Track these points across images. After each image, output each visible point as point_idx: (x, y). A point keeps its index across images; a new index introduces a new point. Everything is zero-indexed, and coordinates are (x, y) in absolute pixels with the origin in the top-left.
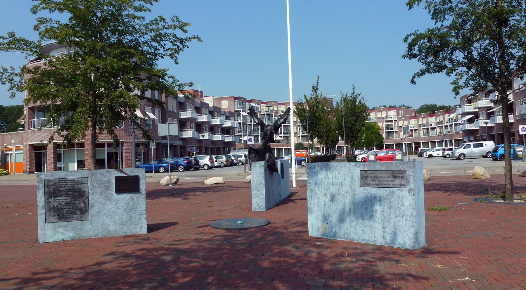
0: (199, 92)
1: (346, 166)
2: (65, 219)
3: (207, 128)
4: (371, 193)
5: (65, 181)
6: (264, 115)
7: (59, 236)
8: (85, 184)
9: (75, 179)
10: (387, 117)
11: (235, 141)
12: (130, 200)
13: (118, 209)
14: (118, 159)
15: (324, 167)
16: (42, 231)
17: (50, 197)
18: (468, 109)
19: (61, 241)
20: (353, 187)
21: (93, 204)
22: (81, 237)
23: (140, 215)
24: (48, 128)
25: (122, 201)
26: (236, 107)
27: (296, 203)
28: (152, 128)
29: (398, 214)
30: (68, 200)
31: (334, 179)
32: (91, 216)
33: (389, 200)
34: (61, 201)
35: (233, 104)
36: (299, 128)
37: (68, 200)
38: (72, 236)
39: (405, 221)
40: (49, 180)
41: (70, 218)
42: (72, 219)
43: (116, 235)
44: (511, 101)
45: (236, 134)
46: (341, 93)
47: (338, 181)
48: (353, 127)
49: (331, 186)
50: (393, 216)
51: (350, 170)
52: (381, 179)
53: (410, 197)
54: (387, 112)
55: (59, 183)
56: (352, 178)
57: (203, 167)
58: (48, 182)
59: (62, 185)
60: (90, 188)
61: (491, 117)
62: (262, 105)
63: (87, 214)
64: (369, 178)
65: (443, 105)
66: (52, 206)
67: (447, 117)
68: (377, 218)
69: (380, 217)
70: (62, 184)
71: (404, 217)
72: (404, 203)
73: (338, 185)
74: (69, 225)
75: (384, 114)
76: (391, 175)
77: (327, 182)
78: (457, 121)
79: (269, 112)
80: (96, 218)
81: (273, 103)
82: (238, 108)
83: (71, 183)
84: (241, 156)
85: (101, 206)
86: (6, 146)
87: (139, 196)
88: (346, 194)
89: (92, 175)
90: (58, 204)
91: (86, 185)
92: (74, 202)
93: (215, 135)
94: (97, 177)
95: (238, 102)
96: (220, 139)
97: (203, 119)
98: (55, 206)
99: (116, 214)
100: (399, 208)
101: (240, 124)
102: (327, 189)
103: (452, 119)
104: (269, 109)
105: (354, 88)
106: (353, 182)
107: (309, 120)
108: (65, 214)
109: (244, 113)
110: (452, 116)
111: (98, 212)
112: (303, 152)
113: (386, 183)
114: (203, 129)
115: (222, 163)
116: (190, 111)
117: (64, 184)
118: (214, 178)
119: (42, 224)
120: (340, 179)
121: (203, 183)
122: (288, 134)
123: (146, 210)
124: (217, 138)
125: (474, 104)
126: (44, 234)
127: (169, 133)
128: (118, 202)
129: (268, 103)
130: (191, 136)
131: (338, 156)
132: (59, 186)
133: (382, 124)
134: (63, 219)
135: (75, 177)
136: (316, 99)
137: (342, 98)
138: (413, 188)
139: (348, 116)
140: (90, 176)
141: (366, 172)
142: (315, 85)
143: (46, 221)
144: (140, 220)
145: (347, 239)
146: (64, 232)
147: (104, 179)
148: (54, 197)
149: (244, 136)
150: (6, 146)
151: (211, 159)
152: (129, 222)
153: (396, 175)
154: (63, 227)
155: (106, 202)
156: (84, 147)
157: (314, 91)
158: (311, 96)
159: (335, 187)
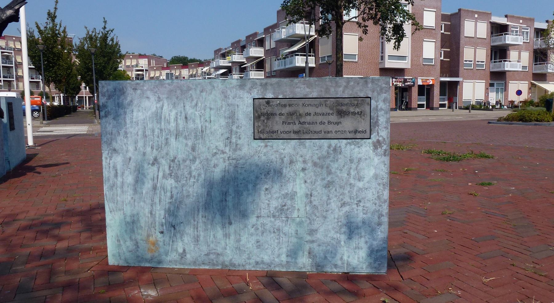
1: (214, 87)
4: (282, 154)
10: (137, 66)
15: (151, 90)
18: (223, 62)
20: (234, 140)
27: (39, 173)
29: (347, 199)
31: (181, 122)
33: (327, 168)
39: (364, 214)
44: (263, 58)
46: (86, 28)
47: (191, 125)
48: (104, 70)
49: (172, 140)
50: (334, 205)
51: (226, 97)
52: (308, 119)
53: (376, 160)
54: (137, 60)
56: (232, 118)
61: (244, 72)
64: (277, 118)
65: (194, 59)
67: (199, 69)
68: (296, 211)
69: (302, 210)
71: (361, 204)
72: (362, 174)
73: (193, 138)
75: (134, 62)
76: (331, 108)
77: (161, 130)
78: (210, 75)
88: (214, 158)
100: (351, 184)
102: (159, 148)
103: (205, 73)
105: (105, 22)
106: (234, 128)
107: (43, 57)
110: (205, 69)
112: (35, 99)
113: (318, 128)
120: (198, 121)
122: (10, 78)
125: (229, 58)
131: (79, 107)
133: (132, 73)
136: (53, 29)
137: (87, 35)
138: (384, 139)
139: (97, 56)
141: (268, 103)
142: (52, 11)
145: (214, 265)
153: (344, 108)
157: (50, 19)
158: (45, 25)
159: (184, 141)
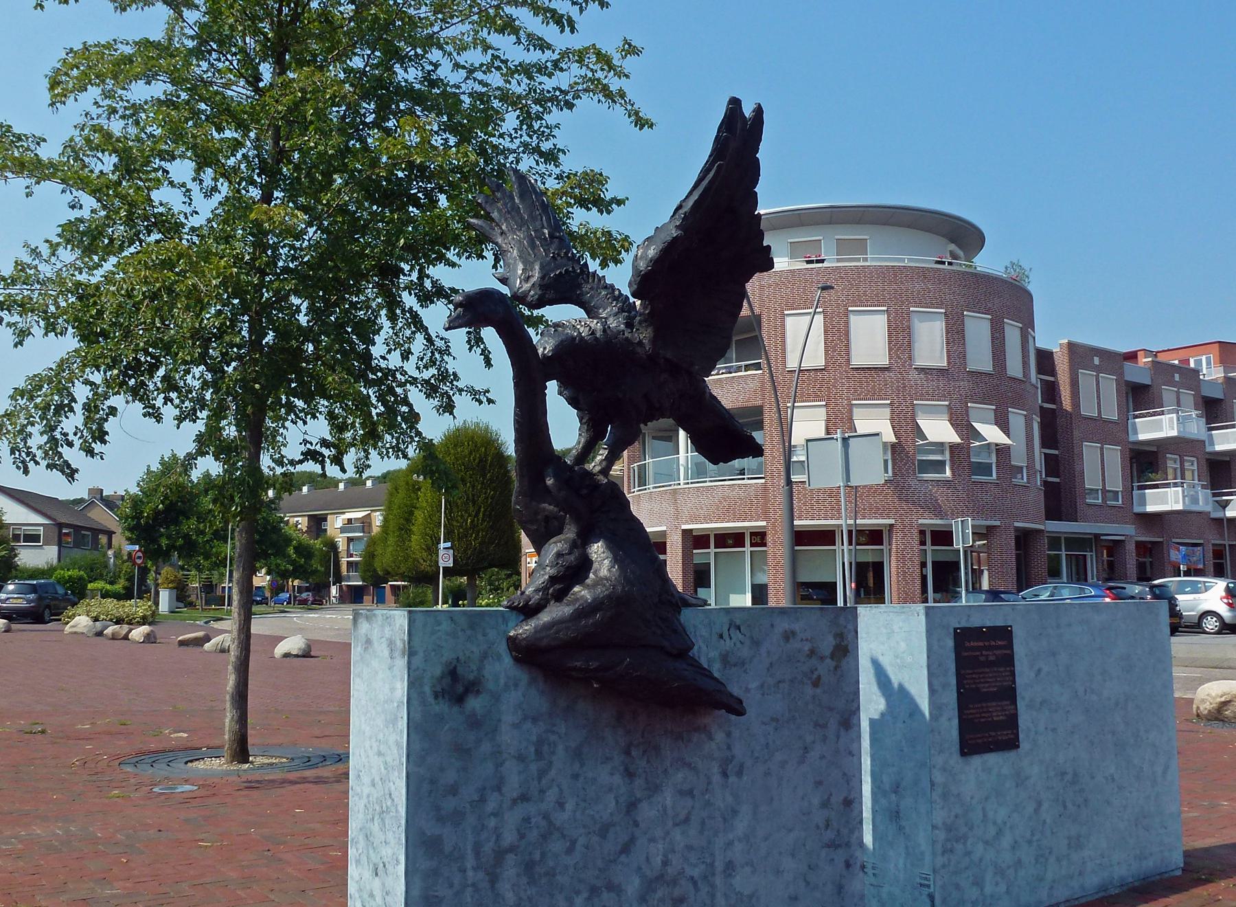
14: (853, 585)
70: (983, 715)
130: (1179, 507)
156: (764, 545)
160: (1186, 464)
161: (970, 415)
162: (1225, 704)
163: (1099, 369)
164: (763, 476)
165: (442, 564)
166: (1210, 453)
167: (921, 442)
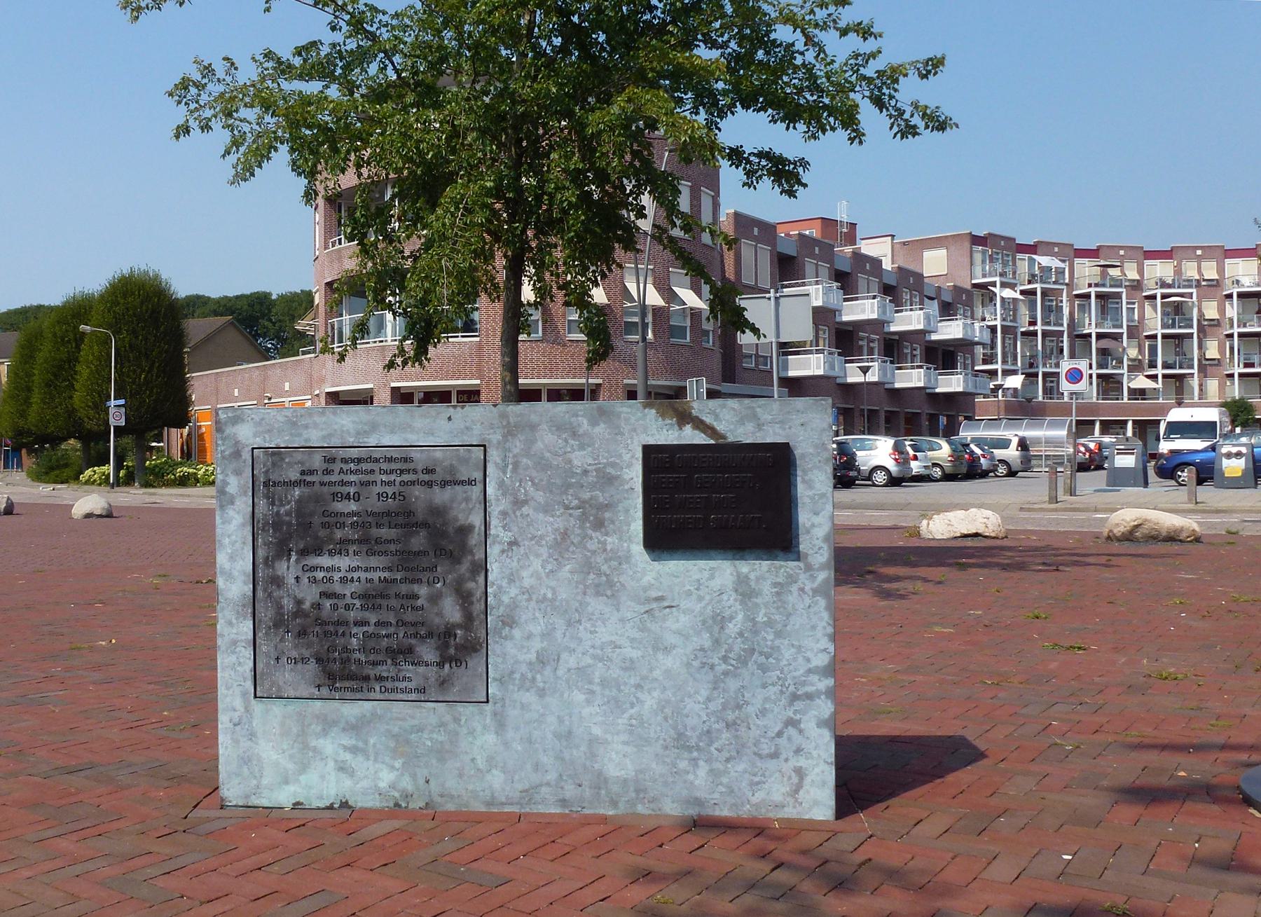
0: (841, 226)
2: (354, 684)
3: (875, 345)
5: (359, 460)
6: (1087, 296)
7: (323, 777)
8: (470, 482)
9: (415, 454)
11: (973, 391)
12: (730, 599)
13: (656, 648)
16: (236, 742)
17: (282, 550)
19: (331, 807)
21: (514, 605)
22: (442, 796)
23: (795, 697)
24: (378, 344)
25: (684, 604)
26: (978, 270)
28: (692, 341)
30: (376, 576)
32: (500, 681)
34: (337, 576)
35: (967, 260)
36: (1232, 349)
37: (376, 576)
38: (393, 786)
40: (277, 454)
41: (380, 679)
42: (392, 690)
43: (640, 809)
45: (976, 368)
55: (328, 472)
57: (869, 478)
58: (274, 464)
59: (343, 483)
60: (494, 510)
62: (1077, 261)
63: (475, 662)
66: (288, 605)
74: (375, 716)
79: (1104, 285)
80: (529, 697)
81: (1122, 252)
82: (984, 276)
83: (392, 477)
84: (1004, 444)
85: (560, 623)
86: (270, 399)
87: (792, 579)
89: (510, 431)
90: (324, 595)
91: (476, 491)
92: (404, 588)
93: (900, 368)
94: (540, 445)
95: (984, 252)
96: (921, 384)
97: (863, 311)
98: (307, 605)
99: (644, 678)
101: (993, 329)
104: (1104, 275)
108: (357, 655)
109: (1008, 293)
111: (542, 660)
114: (861, 347)
115: (935, 465)
116: (817, 283)
117: (353, 478)
118: (960, 513)
119: (238, 703)
121: (916, 533)
122: (1181, 367)
123: (832, 669)
124: (912, 377)
126: (246, 760)
127: (778, 336)
128: (659, 604)
129: (1101, 253)
130: (820, 372)
132: (325, 489)
134: (347, 684)
135: (413, 439)
140: (495, 437)
143: (261, 688)
144: (791, 731)
146: (348, 756)
147: (580, 459)
148: (304, 553)
149: (1007, 373)
150: (270, 399)
151: (898, 449)
152: (726, 735)
154: (344, 730)
155: (588, 599)
160: (821, 332)
161: (671, 279)
162: (1137, 526)
163: (757, 240)
164: (477, 334)
165: (113, 422)
166: (838, 323)
167: (629, 305)
